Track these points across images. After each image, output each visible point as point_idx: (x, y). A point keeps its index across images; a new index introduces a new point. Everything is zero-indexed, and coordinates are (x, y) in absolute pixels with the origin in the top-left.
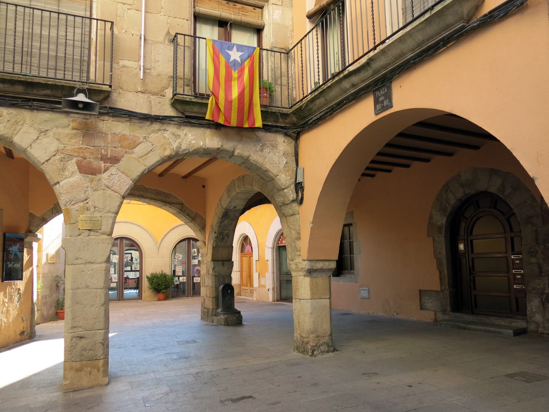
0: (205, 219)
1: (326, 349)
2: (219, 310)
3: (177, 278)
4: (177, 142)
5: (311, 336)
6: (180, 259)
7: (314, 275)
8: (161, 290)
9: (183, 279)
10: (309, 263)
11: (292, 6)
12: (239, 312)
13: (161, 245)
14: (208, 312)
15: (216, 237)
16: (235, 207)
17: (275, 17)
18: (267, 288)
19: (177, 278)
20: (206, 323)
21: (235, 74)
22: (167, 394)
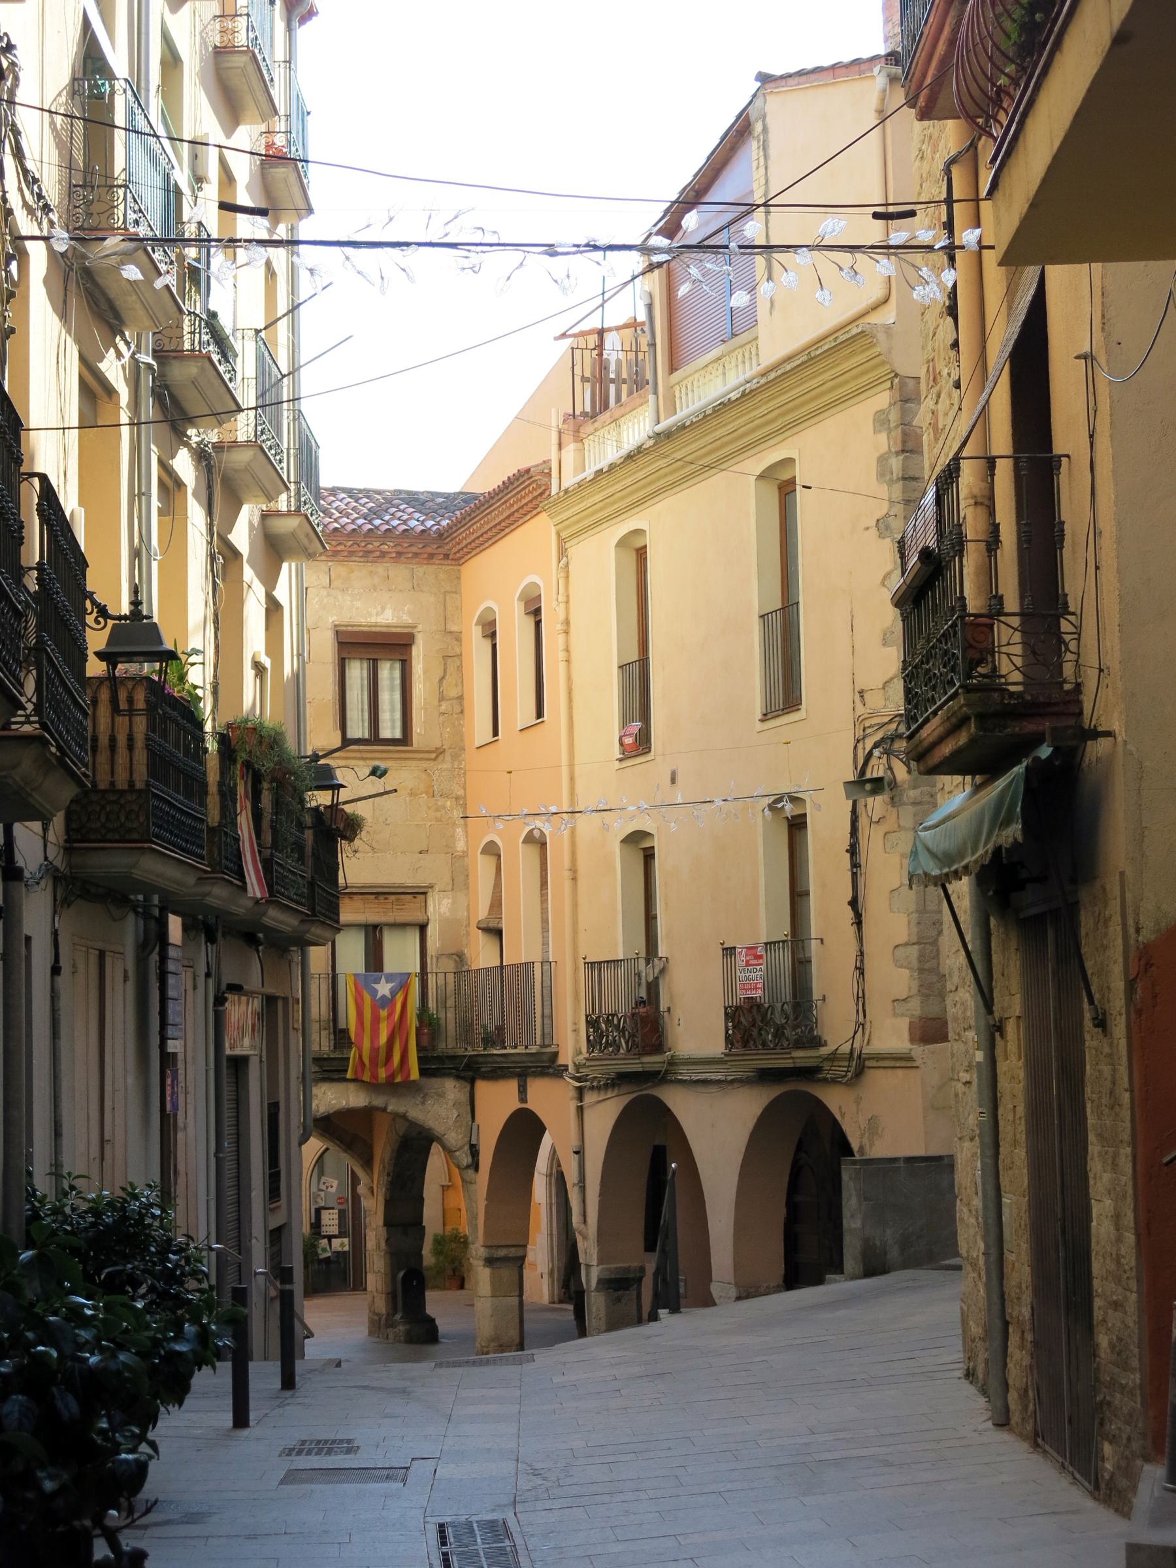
2: (398, 1317)
5: (492, 1344)
6: (333, 1190)
9: (342, 1245)
10: (487, 1250)
11: (468, 888)
12: (433, 1320)
14: (380, 1319)
17: (442, 910)
18: (539, 1271)
21: (384, 1013)
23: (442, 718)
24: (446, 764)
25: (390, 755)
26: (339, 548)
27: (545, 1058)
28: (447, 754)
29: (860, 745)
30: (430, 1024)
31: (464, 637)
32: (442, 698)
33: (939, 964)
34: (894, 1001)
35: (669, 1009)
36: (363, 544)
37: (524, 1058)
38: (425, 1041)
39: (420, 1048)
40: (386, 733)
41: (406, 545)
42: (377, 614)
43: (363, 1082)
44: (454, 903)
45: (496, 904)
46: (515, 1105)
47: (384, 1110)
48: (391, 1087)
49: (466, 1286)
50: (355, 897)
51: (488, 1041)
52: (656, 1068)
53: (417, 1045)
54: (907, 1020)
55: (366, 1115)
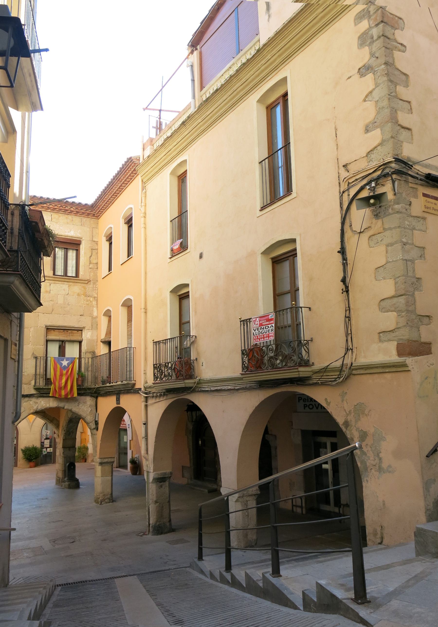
0: (59, 421)
1: (109, 501)
2: (66, 479)
3: (45, 449)
4: (36, 406)
7: (104, 465)
8: (32, 460)
9: (50, 450)
11: (97, 329)
13: (33, 424)
14: (60, 479)
15: (65, 434)
16: (76, 417)
17: (88, 336)
19: (45, 449)
20: (58, 487)
21: (64, 372)
22: (28, 521)
23: (90, 270)
24: (91, 286)
25: (71, 281)
26: (55, 207)
27: (130, 386)
28: (92, 282)
29: (345, 195)
30: (82, 377)
31: (99, 243)
32: (90, 263)
33: (415, 308)
34: (379, 333)
35: (196, 359)
36: (64, 207)
37: (120, 387)
38: (80, 383)
39: (78, 385)
40: (69, 274)
41: (80, 209)
42: (68, 232)
43: (56, 397)
44: (92, 334)
45: (109, 333)
46: (115, 405)
47: (63, 408)
48: (66, 399)
49: (87, 461)
50: (56, 330)
51: (104, 382)
52: (191, 385)
53: (77, 385)
54: (396, 343)
55: (57, 409)
